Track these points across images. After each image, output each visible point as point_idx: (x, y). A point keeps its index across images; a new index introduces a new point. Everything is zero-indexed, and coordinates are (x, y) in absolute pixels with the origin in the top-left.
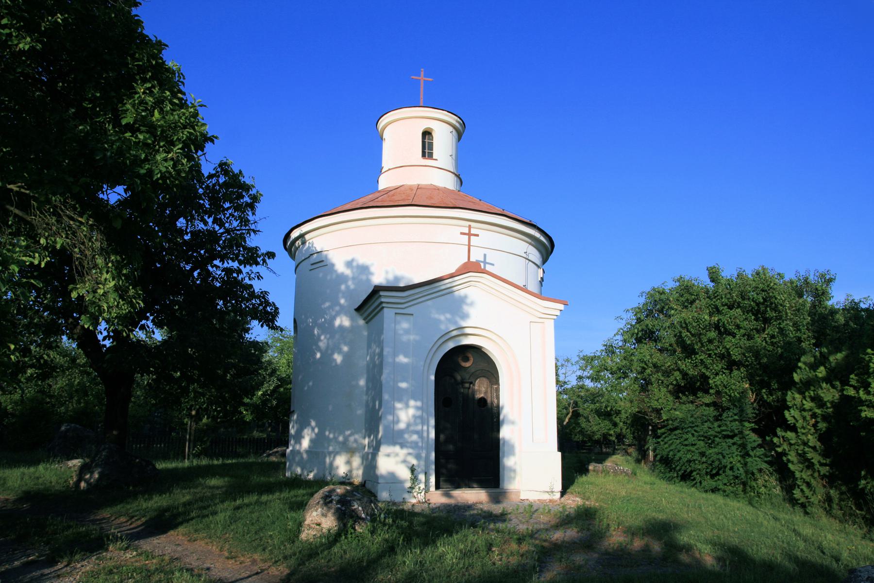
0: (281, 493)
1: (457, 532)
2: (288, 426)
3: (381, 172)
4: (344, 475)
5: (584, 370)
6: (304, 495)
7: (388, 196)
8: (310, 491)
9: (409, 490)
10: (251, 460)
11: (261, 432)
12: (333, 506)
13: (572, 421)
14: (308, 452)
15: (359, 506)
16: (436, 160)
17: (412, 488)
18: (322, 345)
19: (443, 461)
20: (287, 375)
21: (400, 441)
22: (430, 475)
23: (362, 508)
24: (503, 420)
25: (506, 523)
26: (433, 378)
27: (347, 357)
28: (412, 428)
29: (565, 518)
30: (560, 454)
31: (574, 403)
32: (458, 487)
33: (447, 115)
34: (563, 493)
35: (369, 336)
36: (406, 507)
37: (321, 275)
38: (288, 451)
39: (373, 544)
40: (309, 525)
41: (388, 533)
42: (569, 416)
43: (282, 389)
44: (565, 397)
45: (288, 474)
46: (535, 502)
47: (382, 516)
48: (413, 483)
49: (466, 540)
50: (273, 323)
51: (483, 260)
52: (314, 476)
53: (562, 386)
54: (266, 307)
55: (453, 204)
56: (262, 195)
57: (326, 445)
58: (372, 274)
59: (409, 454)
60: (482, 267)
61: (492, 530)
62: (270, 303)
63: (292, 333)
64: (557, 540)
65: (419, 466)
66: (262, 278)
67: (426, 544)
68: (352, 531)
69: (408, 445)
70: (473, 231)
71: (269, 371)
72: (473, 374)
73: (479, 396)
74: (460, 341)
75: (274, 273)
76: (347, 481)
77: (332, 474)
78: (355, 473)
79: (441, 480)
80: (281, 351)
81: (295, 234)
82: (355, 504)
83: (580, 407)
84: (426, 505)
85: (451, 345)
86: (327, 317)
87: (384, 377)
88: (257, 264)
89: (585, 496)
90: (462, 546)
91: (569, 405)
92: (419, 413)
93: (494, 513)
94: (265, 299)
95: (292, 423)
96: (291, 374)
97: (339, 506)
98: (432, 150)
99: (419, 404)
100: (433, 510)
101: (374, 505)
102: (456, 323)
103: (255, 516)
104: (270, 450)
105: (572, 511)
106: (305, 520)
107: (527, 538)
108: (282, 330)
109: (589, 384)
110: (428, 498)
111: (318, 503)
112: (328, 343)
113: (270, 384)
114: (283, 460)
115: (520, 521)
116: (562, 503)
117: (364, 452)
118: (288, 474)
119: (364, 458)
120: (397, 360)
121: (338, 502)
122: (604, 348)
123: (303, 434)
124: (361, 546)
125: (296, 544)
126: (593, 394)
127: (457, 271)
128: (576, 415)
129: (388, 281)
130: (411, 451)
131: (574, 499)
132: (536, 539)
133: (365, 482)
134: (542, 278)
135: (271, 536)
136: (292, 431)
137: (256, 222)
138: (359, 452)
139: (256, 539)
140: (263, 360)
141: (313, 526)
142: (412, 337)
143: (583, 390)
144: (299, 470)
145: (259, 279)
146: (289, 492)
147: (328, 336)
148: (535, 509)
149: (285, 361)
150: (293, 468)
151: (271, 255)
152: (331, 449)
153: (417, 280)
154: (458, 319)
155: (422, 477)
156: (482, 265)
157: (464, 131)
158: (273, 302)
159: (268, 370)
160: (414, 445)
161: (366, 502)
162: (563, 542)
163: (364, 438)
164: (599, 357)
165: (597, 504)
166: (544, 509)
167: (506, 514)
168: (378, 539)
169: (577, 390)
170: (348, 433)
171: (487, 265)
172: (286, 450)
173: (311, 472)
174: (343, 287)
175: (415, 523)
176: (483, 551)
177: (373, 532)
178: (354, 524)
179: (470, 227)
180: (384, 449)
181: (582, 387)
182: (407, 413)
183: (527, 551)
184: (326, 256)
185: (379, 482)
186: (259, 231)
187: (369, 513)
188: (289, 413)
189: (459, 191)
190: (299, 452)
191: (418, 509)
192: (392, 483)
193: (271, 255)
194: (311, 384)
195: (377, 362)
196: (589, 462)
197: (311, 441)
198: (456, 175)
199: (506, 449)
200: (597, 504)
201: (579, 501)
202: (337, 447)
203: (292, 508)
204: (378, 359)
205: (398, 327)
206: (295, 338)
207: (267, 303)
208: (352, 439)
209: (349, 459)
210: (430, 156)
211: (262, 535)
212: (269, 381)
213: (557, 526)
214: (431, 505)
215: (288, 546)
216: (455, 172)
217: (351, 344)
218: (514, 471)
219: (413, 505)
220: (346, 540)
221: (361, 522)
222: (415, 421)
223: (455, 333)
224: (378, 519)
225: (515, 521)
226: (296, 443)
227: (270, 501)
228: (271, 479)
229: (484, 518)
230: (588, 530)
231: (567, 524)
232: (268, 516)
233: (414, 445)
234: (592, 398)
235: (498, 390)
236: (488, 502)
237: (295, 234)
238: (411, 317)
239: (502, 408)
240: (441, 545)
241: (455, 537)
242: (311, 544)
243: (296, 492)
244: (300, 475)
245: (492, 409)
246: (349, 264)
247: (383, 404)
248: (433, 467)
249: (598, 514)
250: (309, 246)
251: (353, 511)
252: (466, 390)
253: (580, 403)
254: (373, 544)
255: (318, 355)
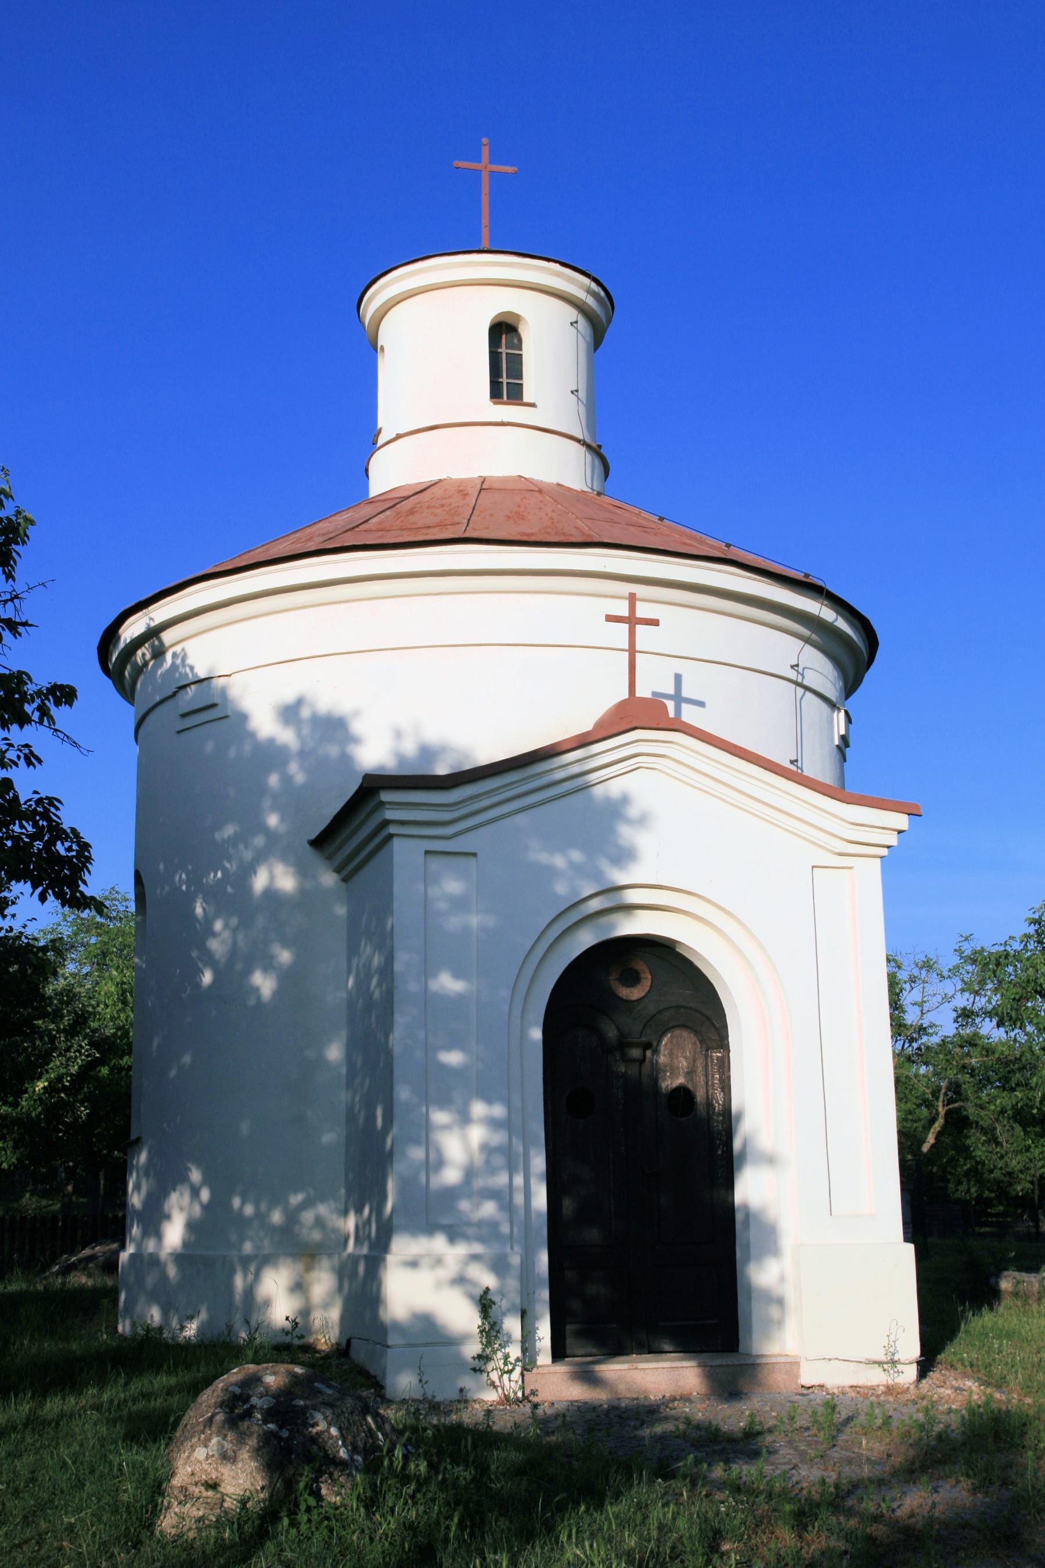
0: (102, 1390)
1: (617, 1496)
2: (125, 1184)
3: (375, 443)
4: (288, 1325)
5: (977, 993)
6: (169, 1392)
7: (398, 515)
8: (186, 1377)
9: (477, 1364)
10: (13, 1288)
11: (45, 1194)
12: (256, 1428)
13: (947, 1140)
14: (181, 1258)
15: (330, 1425)
16: (533, 405)
17: (484, 1357)
18: (216, 946)
19: (570, 1275)
20: (118, 1029)
21: (445, 1221)
22: (536, 1318)
23: (340, 1429)
24: (743, 1154)
25: (760, 1462)
26: (537, 1034)
27: (288, 979)
28: (479, 1183)
29: (933, 1443)
30: (911, 1248)
31: (948, 1089)
32: (617, 1350)
33: (558, 275)
34: (925, 1366)
35: (353, 919)
36: (470, 1416)
37: (209, 747)
38: (124, 1256)
39: (372, 1539)
40: (183, 1489)
41: (415, 1504)
42: (937, 1126)
43: (105, 1071)
44: (923, 1070)
45: (124, 1327)
46: (844, 1394)
47: (398, 1452)
48: (489, 1344)
49: (645, 1517)
50: (74, 887)
51: (671, 691)
52: (200, 1330)
53: (912, 1040)
54: (52, 842)
55: (583, 534)
56: (33, 523)
57: (234, 1237)
58: (356, 740)
59: (475, 1258)
60: (672, 714)
61: (721, 1485)
62: (65, 832)
63: (132, 908)
64: (912, 1515)
65: (502, 1293)
66: (40, 761)
67: (527, 1535)
68: (312, 1502)
69: (470, 1231)
70: (643, 611)
71: (66, 1021)
72: (652, 1018)
73: (669, 1083)
74: (612, 927)
75: (75, 744)
76: (296, 1342)
77: (253, 1323)
78: (317, 1318)
79: (568, 1333)
80: (101, 959)
81: (132, 629)
82: (319, 1417)
83: (967, 1099)
84: (527, 1408)
85: (586, 939)
86: (231, 866)
87: (397, 1039)
88: (23, 720)
89: (990, 1375)
90: (631, 1542)
91: (935, 1093)
92: (499, 1138)
93: (725, 1428)
94: (50, 820)
95: (134, 1175)
96: (131, 1024)
97: (271, 1426)
98: (520, 377)
99: (498, 1111)
100: (544, 1423)
101: (374, 1418)
102: (598, 875)
103: (22, 1465)
104: (72, 1253)
105: (954, 1421)
106: (173, 1475)
107: (824, 1514)
108: (99, 906)
109: (990, 1030)
110: (532, 1387)
111: (211, 1420)
112: (235, 942)
113: (68, 1060)
114: (110, 1282)
115: (802, 1454)
116: (923, 1398)
117: (345, 1254)
118: (124, 1327)
119: (344, 1273)
120: (434, 986)
121: (270, 1415)
122: (1032, 929)
123: (166, 1207)
124: (337, 1550)
125: (146, 1550)
126: (1005, 1062)
127: (600, 725)
128: (957, 1122)
129: (402, 759)
130: (478, 1248)
131: (959, 1383)
132: (850, 1513)
133: (349, 1342)
134: (844, 739)
135: (71, 1528)
136: (136, 1200)
137: (16, 597)
138: (330, 1255)
139: (26, 1542)
140: (49, 990)
141: (196, 1490)
142: (474, 920)
143: (975, 1052)
144: (155, 1315)
145: (29, 763)
146: (127, 1384)
147: (234, 921)
148: (844, 1416)
149: (113, 989)
150: (138, 1308)
151: (65, 694)
152: (248, 1247)
153: (487, 754)
154: (604, 865)
155: (512, 1325)
156: (670, 705)
157: (609, 320)
158: (73, 830)
159: (62, 1017)
160: (487, 1232)
161: (352, 1412)
162: (931, 1520)
163: (345, 1213)
164: (1017, 956)
165: (1028, 1400)
166: (871, 1415)
167: (759, 1433)
168: (388, 1525)
169: (958, 1050)
170: (296, 1199)
171: (685, 707)
172: (116, 1254)
173: (191, 1318)
174: (274, 780)
175: (493, 1467)
176: (693, 1553)
177: (371, 1503)
178: (316, 1480)
179: (632, 599)
180: (402, 1247)
181: (971, 1042)
182: (465, 1139)
183: (823, 1553)
184: (223, 692)
185: (390, 1343)
186: (25, 624)
187: (360, 1444)
188: (129, 1144)
189: (599, 494)
190: (154, 1261)
191: (502, 1424)
192: (427, 1345)
193: (65, 694)
194: (187, 1059)
195: (377, 994)
196: (1000, 1267)
197: (191, 1226)
198: (589, 447)
199: (753, 1236)
200: (1028, 1400)
201: (973, 1390)
202: (266, 1243)
203: (132, 1437)
204: (379, 984)
205: (434, 891)
206: (141, 927)
207: (57, 832)
208: (308, 1217)
209: (302, 1277)
210: (515, 395)
211: (43, 1525)
212: (68, 1050)
213: (912, 1472)
214: (540, 1411)
215: (123, 1557)
216: (588, 440)
217: (296, 942)
218: (780, 1302)
219: (488, 1412)
220: (293, 1531)
221: (336, 1474)
222: (487, 1162)
223: (595, 905)
224: (386, 1463)
225: (785, 1454)
226: (145, 1234)
227: (71, 1415)
228: (74, 1346)
229: (697, 1445)
230: (1005, 1483)
231: (942, 1462)
232: (64, 1464)
233: (487, 1232)
234: (1003, 1071)
235: (724, 1065)
236: (707, 1396)
237: (132, 629)
238: (472, 861)
239: (740, 1116)
240: (570, 1536)
241: (611, 1510)
242: (189, 1547)
243: (146, 1382)
244: (160, 1329)
245: (709, 1118)
246: (290, 713)
247: (397, 1111)
248: (545, 1294)
249: (1031, 1434)
250: (173, 664)
251: (314, 1440)
252: (633, 1070)
253: (968, 1090)
254: (372, 1539)
255: (207, 978)
